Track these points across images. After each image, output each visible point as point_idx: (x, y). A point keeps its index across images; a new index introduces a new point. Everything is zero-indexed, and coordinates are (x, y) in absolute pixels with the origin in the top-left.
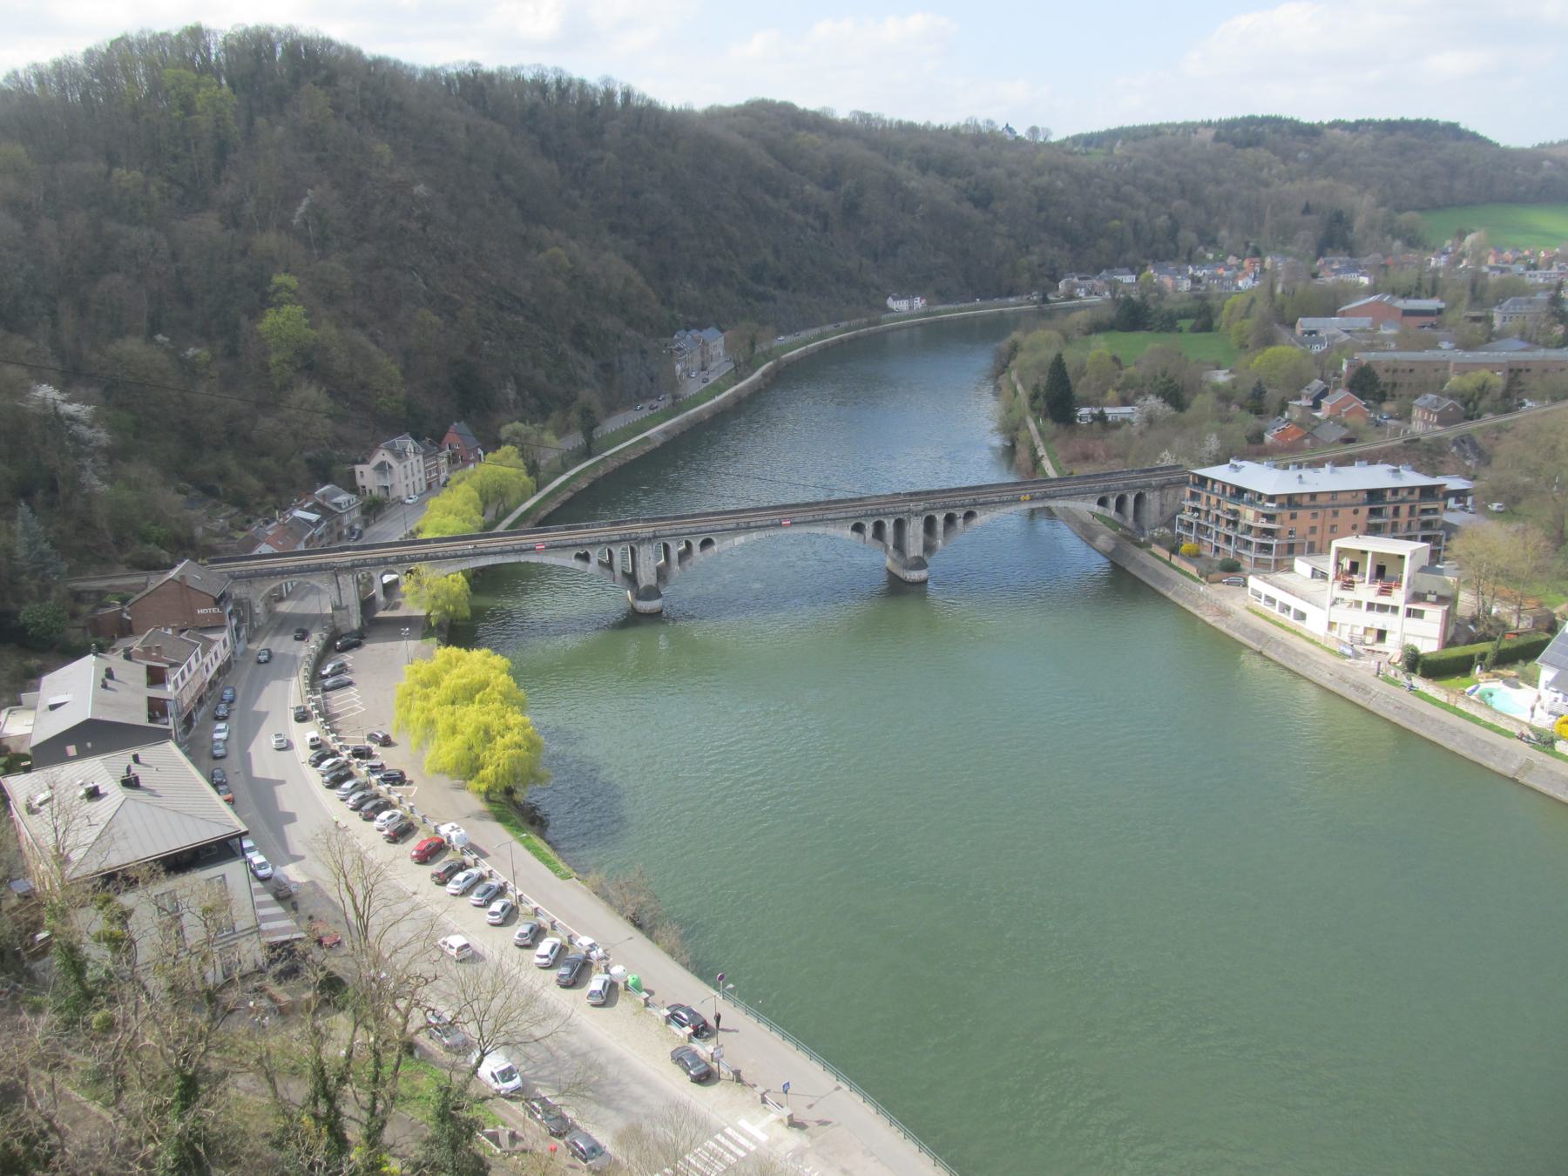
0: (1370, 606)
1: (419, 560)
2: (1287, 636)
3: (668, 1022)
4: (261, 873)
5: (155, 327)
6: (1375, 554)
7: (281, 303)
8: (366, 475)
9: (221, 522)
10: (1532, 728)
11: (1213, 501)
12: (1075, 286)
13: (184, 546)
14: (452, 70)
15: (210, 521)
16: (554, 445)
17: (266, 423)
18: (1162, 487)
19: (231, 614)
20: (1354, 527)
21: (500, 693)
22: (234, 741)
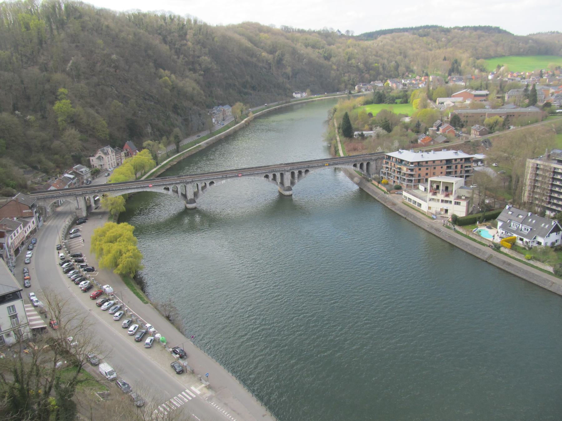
0: (442, 201)
3: (171, 353)
4: (36, 304)
5: (15, 108)
6: (443, 182)
7: (62, 99)
8: (94, 161)
9: (39, 179)
10: (493, 243)
11: (393, 165)
12: (361, 88)
13: (23, 188)
14: (130, 13)
15: (32, 179)
16: (162, 150)
17: (56, 143)
18: (376, 160)
19: (36, 212)
20: (441, 173)
21: (127, 238)
22: (34, 257)
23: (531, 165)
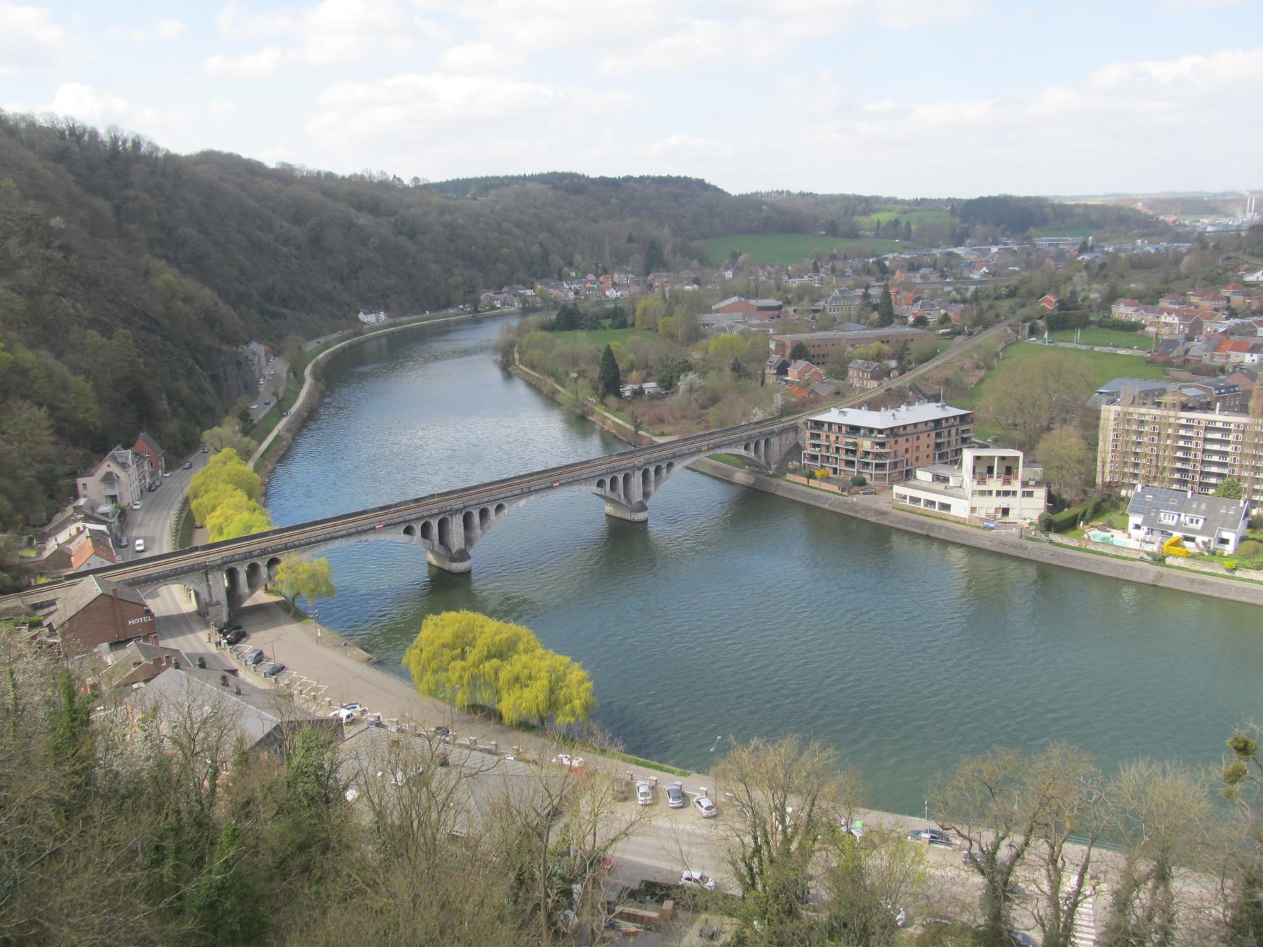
0: (998, 493)
11: (832, 438)
12: (492, 299)
23: (1112, 416)
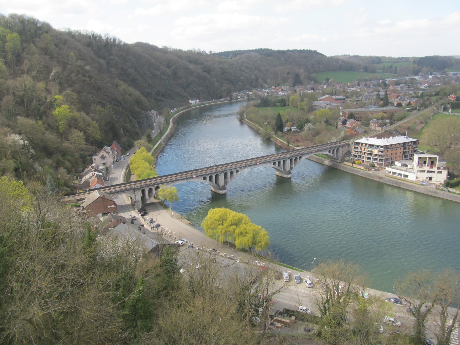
0: (428, 172)
1: (160, 184)
2: (404, 182)
12: (237, 95)
